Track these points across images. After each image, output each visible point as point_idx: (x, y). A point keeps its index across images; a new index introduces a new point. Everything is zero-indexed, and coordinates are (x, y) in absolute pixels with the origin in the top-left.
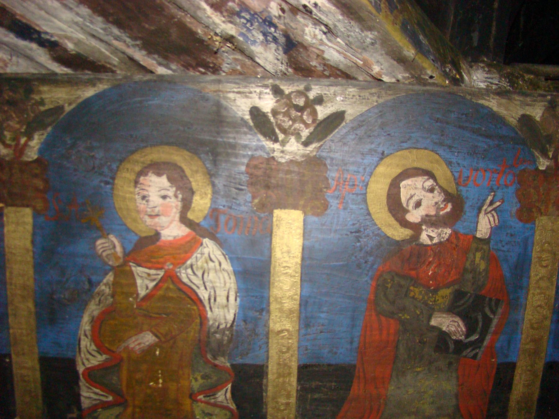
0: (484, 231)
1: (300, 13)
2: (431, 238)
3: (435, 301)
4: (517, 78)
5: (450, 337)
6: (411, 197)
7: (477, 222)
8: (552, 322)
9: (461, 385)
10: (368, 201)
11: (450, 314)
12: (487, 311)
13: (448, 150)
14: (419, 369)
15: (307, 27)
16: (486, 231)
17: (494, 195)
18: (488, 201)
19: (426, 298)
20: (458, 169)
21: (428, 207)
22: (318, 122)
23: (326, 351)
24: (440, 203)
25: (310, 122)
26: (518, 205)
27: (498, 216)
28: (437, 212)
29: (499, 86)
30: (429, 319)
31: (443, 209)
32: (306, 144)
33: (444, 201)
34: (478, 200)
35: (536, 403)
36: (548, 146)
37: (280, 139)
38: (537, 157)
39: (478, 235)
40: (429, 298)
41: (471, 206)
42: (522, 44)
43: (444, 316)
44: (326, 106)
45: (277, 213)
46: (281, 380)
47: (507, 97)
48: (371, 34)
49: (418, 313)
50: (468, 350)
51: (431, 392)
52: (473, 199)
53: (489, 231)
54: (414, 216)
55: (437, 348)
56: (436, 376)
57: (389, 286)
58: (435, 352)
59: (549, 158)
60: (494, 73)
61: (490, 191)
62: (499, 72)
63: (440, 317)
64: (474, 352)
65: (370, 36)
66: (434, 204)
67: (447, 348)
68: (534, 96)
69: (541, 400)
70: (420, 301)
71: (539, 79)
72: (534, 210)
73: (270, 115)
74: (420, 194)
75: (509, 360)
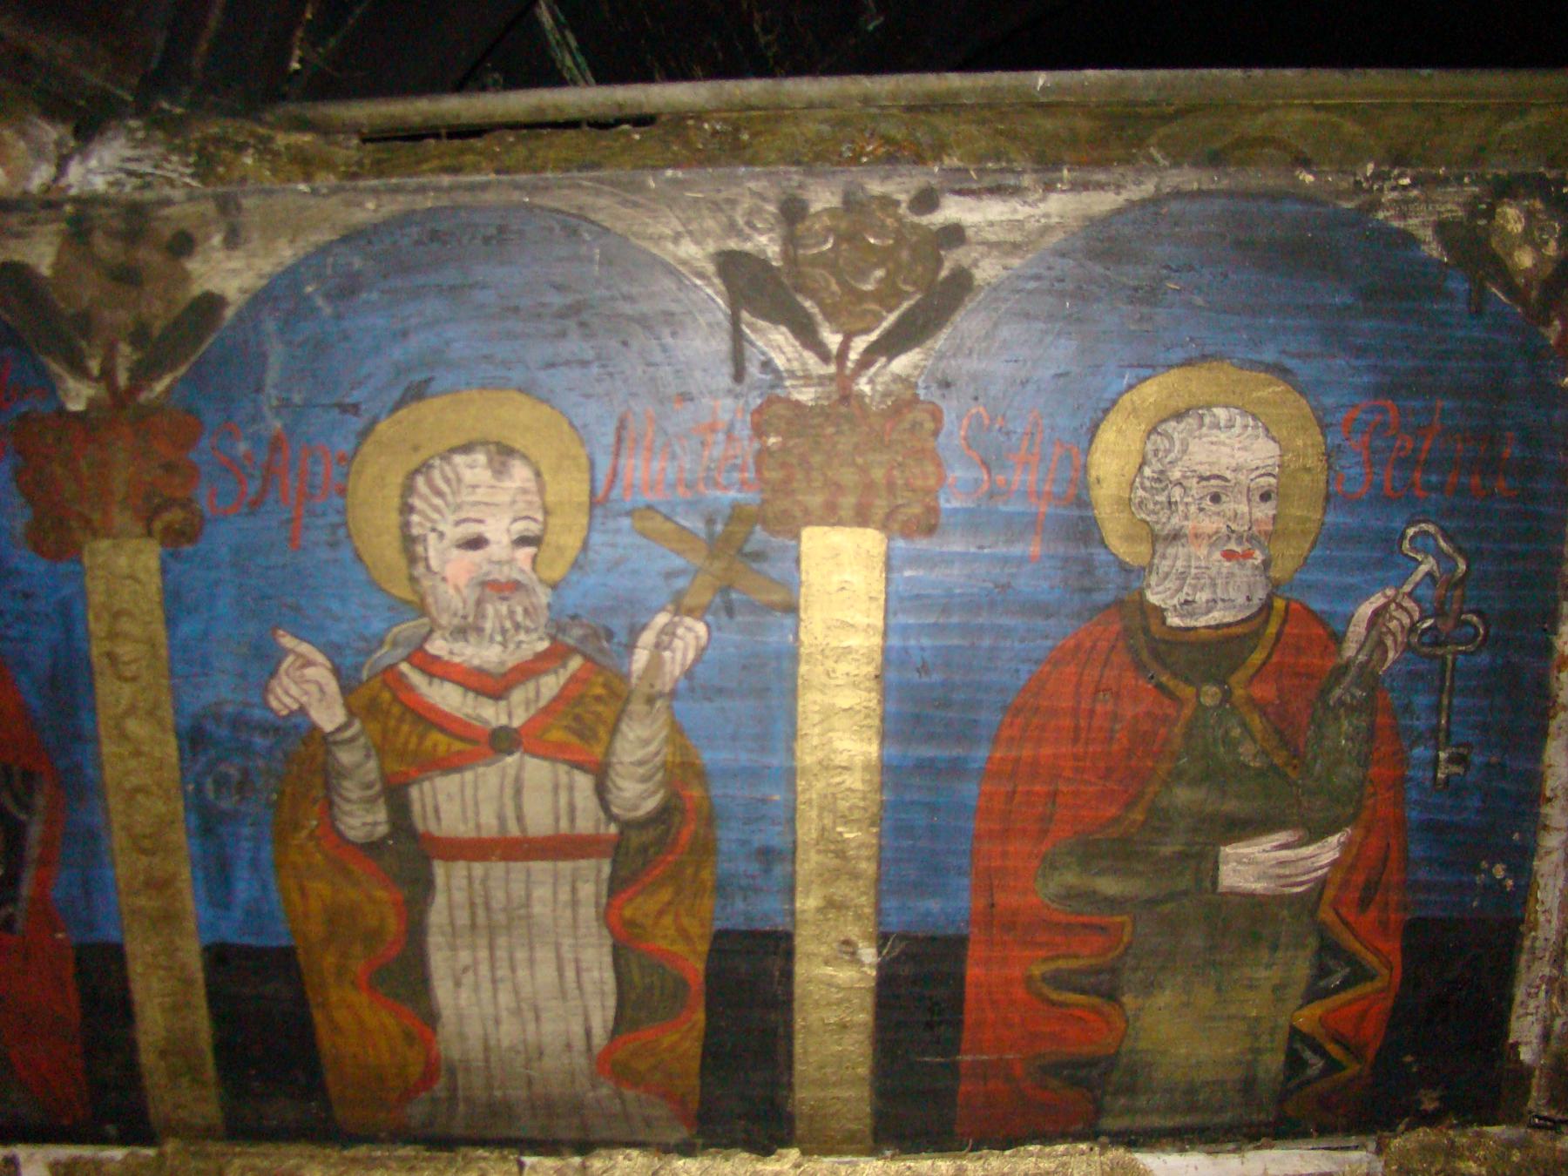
4: (240, 148)
29: (149, 179)
36: (83, 344)
68: (28, 211)
69: (223, 1048)
72: (74, 524)
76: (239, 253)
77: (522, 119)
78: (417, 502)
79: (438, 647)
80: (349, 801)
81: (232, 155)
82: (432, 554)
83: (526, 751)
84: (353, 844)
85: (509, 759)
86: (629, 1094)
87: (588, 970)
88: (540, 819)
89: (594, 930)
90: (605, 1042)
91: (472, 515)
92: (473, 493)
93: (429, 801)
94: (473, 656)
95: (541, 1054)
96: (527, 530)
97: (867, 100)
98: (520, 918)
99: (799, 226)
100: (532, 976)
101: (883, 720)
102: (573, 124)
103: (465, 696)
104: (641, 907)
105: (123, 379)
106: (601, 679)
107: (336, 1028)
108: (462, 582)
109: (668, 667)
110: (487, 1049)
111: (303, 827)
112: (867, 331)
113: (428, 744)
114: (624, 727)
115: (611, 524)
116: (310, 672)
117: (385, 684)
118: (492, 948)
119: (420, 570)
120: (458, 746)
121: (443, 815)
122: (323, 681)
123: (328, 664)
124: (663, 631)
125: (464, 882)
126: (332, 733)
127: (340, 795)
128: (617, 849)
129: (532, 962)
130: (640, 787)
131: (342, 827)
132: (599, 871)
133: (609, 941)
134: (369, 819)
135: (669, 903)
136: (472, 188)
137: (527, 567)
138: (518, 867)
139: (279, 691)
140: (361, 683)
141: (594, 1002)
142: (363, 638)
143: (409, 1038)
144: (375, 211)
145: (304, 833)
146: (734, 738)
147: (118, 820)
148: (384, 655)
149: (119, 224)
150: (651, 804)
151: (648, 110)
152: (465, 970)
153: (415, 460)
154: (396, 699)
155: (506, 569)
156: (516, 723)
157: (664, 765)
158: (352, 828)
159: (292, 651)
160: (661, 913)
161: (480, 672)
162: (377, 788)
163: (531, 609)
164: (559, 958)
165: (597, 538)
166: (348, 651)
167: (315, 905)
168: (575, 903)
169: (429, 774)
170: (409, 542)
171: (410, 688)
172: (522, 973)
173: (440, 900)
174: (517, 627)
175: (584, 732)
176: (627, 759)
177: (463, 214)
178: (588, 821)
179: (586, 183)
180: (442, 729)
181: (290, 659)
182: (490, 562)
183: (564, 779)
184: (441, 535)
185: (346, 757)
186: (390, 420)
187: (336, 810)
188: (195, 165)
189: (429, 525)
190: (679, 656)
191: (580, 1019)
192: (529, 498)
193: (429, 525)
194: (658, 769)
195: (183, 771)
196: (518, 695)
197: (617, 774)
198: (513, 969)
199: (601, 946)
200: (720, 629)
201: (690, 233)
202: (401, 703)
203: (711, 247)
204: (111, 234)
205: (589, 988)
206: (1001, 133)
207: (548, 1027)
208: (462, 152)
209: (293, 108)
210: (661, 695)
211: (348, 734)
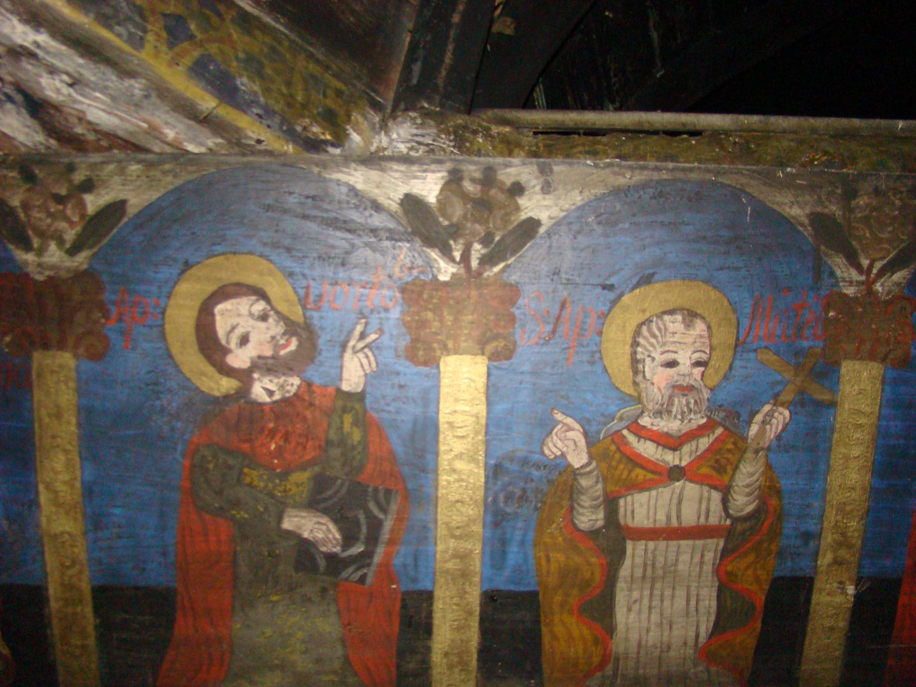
0: (355, 380)
1: (24, 59)
2: (271, 393)
3: (285, 491)
4: (475, 133)
5: (318, 550)
6: (233, 328)
7: (341, 368)
8: (484, 526)
9: (349, 624)
10: (169, 338)
11: (312, 513)
12: (372, 506)
13: (286, 255)
14: (275, 598)
15: (41, 76)
16: (357, 381)
17: (366, 324)
18: (357, 333)
19: (271, 485)
20: (304, 283)
21: (261, 344)
22: (87, 218)
23: (130, 565)
24: (278, 337)
25: (76, 219)
26: (408, 338)
27: (375, 356)
28: (274, 351)
29: (431, 147)
30: (280, 519)
31: (285, 346)
32: (73, 251)
33: (284, 334)
34: (341, 331)
35: (475, 656)
36: (452, 242)
37: (36, 245)
38: (435, 260)
39: (345, 387)
40: (275, 486)
41: (330, 341)
43: (303, 514)
44: (99, 194)
45: (37, 356)
46: (69, 610)
47: (378, 167)
48: (137, 82)
49: (262, 509)
50: (351, 570)
51: (300, 634)
52: (332, 330)
53: (363, 380)
54: (240, 359)
55: (299, 566)
56: (303, 609)
57: (211, 466)
58: (297, 570)
59: (453, 260)
60: (430, 126)
61: (360, 316)
62: (438, 124)
63: (296, 516)
64: (360, 573)
65: (137, 85)
66: (269, 339)
67: (314, 568)
69: (484, 652)
70: (261, 492)
71: (522, 134)
73: (20, 210)
74: (246, 325)
75: (419, 586)
76: (551, 196)
77: (631, 128)
78: (641, 340)
79: (645, 421)
80: (582, 507)
81: (472, 136)
82: (647, 369)
83: (687, 480)
84: (582, 531)
85: (677, 484)
86: (713, 669)
87: (703, 600)
88: (689, 517)
89: (710, 578)
90: (705, 641)
91: (671, 349)
92: (673, 336)
93: (629, 508)
94: (664, 426)
95: (669, 647)
96: (701, 358)
97: (814, 131)
98: (670, 572)
99: (853, 202)
100: (672, 605)
101: (873, 463)
102: (656, 133)
103: (657, 447)
104: (737, 565)
105: (474, 263)
106: (732, 440)
107: (555, 637)
108: (662, 386)
109: (767, 435)
110: (639, 645)
111: (554, 522)
112: (882, 259)
113: (633, 475)
114: (741, 466)
115: (745, 356)
116: (570, 434)
117: (613, 441)
118: (652, 589)
119: (639, 378)
120: (650, 476)
121: (635, 515)
122: (577, 439)
123: (581, 430)
124: (767, 415)
125: (643, 553)
126: (578, 469)
127: (579, 504)
128: (728, 533)
129: (673, 596)
130: (746, 499)
131: (577, 522)
132: (717, 545)
133: (717, 584)
134: (594, 517)
135: (753, 563)
136: (683, 170)
137: (699, 378)
138: (673, 544)
139: (550, 445)
140: (599, 441)
141: (703, 619)
142: (603, 415)
143: (596, 641)
144: (630, 179)
145: (554, 525)
146: (797, 472)
147: (441, 519)
148: (614, 425)
149: (478, 175)
150: (750, 508)
151: (698, 128)
152: (635, 601)
153: (642, 318)
154: (618, 449)
155: (687, 379)
156: (683, 464)
157: (760, 487)
158: (582, 522)
159: (561, 422)
160: (747, 568)
161: (667, 435)
162: (601, 499)
163: (698, 400)
164: (688, 594)
165: (737, 363)
166: (594, 423)
167: (554, 567)
168: (702, 563)
169: (632, 492)
170: (635, 362)
171: (627, 444)
172: (667, 603)
173: (628, 562)
174: (690, 411)
175: (720, 468)
176: (740, 483)
177: (679, 184)
178: (715, 519)
179: (745, 172)
180: (643, 467)
181: (560, 426)
182: (679, 374)
183: (706, 495)
184: (653, 359)
185: (584, 482)
186: (632, 294)
187: (575, 513)
188: (454, 140)
189: (647, 353)
190: (774, 429)
191: (694, 629)
192: (703, 340)
193: (647, 353)
194: (756, 489)
195: (487, 489)
196: (686, 449)
197: (735, 493)
198: (662, 601)
199: (712, 587)
200: (796, 413)
201: (798, 202)
202: (621, 452)
203: (807, 211)
204: (473, 181)
205: (702, 610)
206: (882, 152)
207: (675, 632)
208: (594, 144)
209: (498, 112)
210: (762, 449)
211: (588, 469)
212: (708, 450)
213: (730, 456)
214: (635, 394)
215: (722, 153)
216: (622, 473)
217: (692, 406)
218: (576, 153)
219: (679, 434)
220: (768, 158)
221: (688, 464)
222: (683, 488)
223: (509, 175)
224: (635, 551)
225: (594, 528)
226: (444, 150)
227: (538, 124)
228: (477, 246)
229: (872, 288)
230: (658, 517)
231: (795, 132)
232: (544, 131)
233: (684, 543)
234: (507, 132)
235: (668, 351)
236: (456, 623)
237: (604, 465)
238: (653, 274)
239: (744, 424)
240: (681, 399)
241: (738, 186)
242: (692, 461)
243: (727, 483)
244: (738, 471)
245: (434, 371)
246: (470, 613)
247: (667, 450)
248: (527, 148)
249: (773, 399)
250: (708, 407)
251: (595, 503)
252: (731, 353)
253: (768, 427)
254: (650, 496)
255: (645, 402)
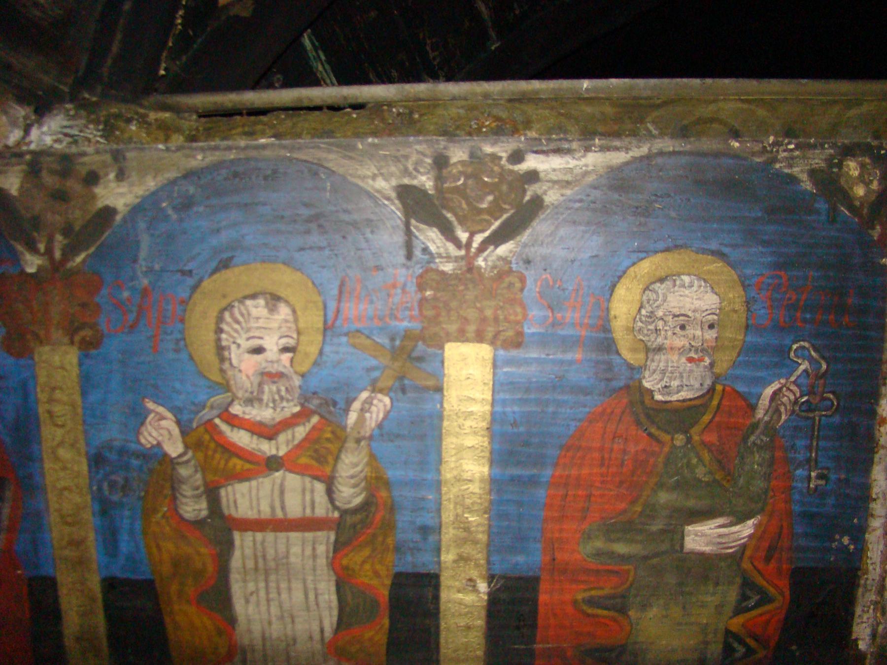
4: (129, 121)
29: (76, 138)
36: (36, 234)
42: (497, 45)
60: (81, 118)
75: (43, 573)
76: (124, 183)
78: (224, 326)
79: (236, 409)
80: (185, 496)
82: (233, 356)
85: (277, 474)
90: (332, 636)
92: (257, 322)
96: (288, 343)
97: (486, 96)
98: (283, 564)
100: (290, 598)
101: (491, 453)
102: (318, 108)
104: (355, 558)
105: (58, 255)
106: (329, 429)
108: (251, 372)
109: (368, 423)
110: (264, 638)
113: (231, 464)
114: (343, 456)
115: (336, 340)
116: (164, 423)
117: (207, 431)
119: (226, 366)
120: (248, 466)
121: (239, 506)
122: (171, 428)
123: (173, 418)
128: (338, 525)
129: (290, 589)
130: (352, 490)
132: (328, 538)
133: (334, 578)
134: (197, 507)
135: (369, 557)
137: (288, 364)
138: (282, 535)
139: (146, 434)
141: (325, 613)
142: (193, 403)
143: (220, 633)
144: (202, 160)
146: (405, 463)
147: (54, 505)
150: (358, 501)
151: (360, 101)
152: (252, 594)
153: (224, 303)
154: (212, 438)
155: (276, 365)
156: (281, 453)
157: (366, 477)
159: (153, 411)
161: (260, 424)
162: (202, 489)
165: (327, 349)
166: (185, 412)
167: (165, 556)
168: (314, 556)
169: (231, 482)
170: (220, 349)
171: (220, 433)
172: (284, 596)
173: (237, 553)
174: (282, 398)
175: (321, 459)
176: (344, 474)
178: (322, 509)
179: (322, 146)
181: (152, 415)
182: (267, 361)
183: (308, 485)
184: (239, 346)
185: (184, 472)
187: (178, 502)
188: (103, 130)
189: (232, 340)
190: (374, 416)
191: (317, 623)
192: (289, 325)
193: (232, 340)
194: (362, 481)
196: (282, 438)
197: (339, 483)
198: (279, 594)
199: (329, 581)
201: (382, 174)
202: (216, 442)
203: (394, 182)
204: (53, 172)
205: (322, 605)
210: (364, 438)
211: (185, 458)
212: (305, 439)
213: (329, 445)
214: (224, 382)
215: (381, 125)
216: (219, 463)
217: (283, 393)
218: (234, 134)
219: (273, 423)
220: (432, 127)
221: (287, 454)
222: (283, 479)
223: (84, 164)
224: (244, 543)
225: (199, 518)
226: (89, 140)
227: (198, 108)
228: (59, 237)
229: (473, 264)
230: (262, 508)
231: (466, 99)
232: (297, 112)
233: (293, 535)
234: (166, 117)
235: (253, 337)
236: (82, 609)
237: (200, 455)
238: (232, 258)
239: (341, 412)
240: (271, 387)
241: (315, 161)
242: (290, 451)
243: (329, 474)
244: (340, 461)
245: (30, 362)
246: (93, 599)
247: (262, 440)
248: (187, 132)
249: (371, 385)
250: (300, 395)
251: (196, 492)
252: (320, 338)
253: (367, 415)
254: (250, 487)
255: (234, 389)
